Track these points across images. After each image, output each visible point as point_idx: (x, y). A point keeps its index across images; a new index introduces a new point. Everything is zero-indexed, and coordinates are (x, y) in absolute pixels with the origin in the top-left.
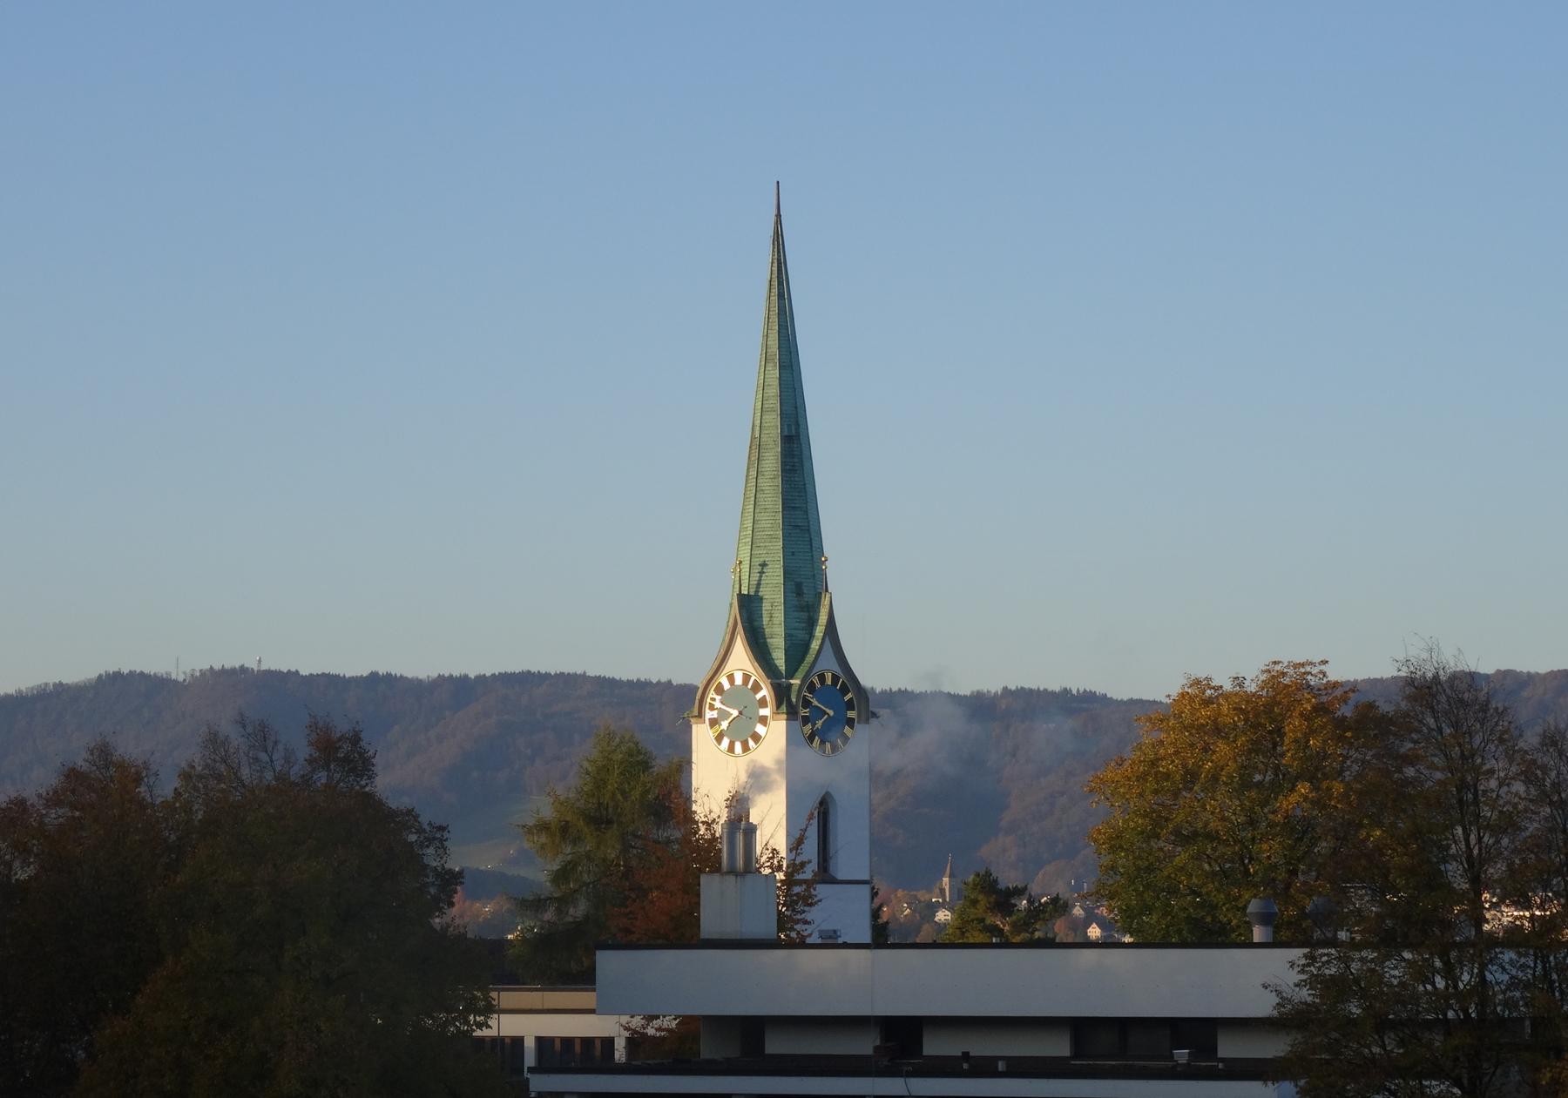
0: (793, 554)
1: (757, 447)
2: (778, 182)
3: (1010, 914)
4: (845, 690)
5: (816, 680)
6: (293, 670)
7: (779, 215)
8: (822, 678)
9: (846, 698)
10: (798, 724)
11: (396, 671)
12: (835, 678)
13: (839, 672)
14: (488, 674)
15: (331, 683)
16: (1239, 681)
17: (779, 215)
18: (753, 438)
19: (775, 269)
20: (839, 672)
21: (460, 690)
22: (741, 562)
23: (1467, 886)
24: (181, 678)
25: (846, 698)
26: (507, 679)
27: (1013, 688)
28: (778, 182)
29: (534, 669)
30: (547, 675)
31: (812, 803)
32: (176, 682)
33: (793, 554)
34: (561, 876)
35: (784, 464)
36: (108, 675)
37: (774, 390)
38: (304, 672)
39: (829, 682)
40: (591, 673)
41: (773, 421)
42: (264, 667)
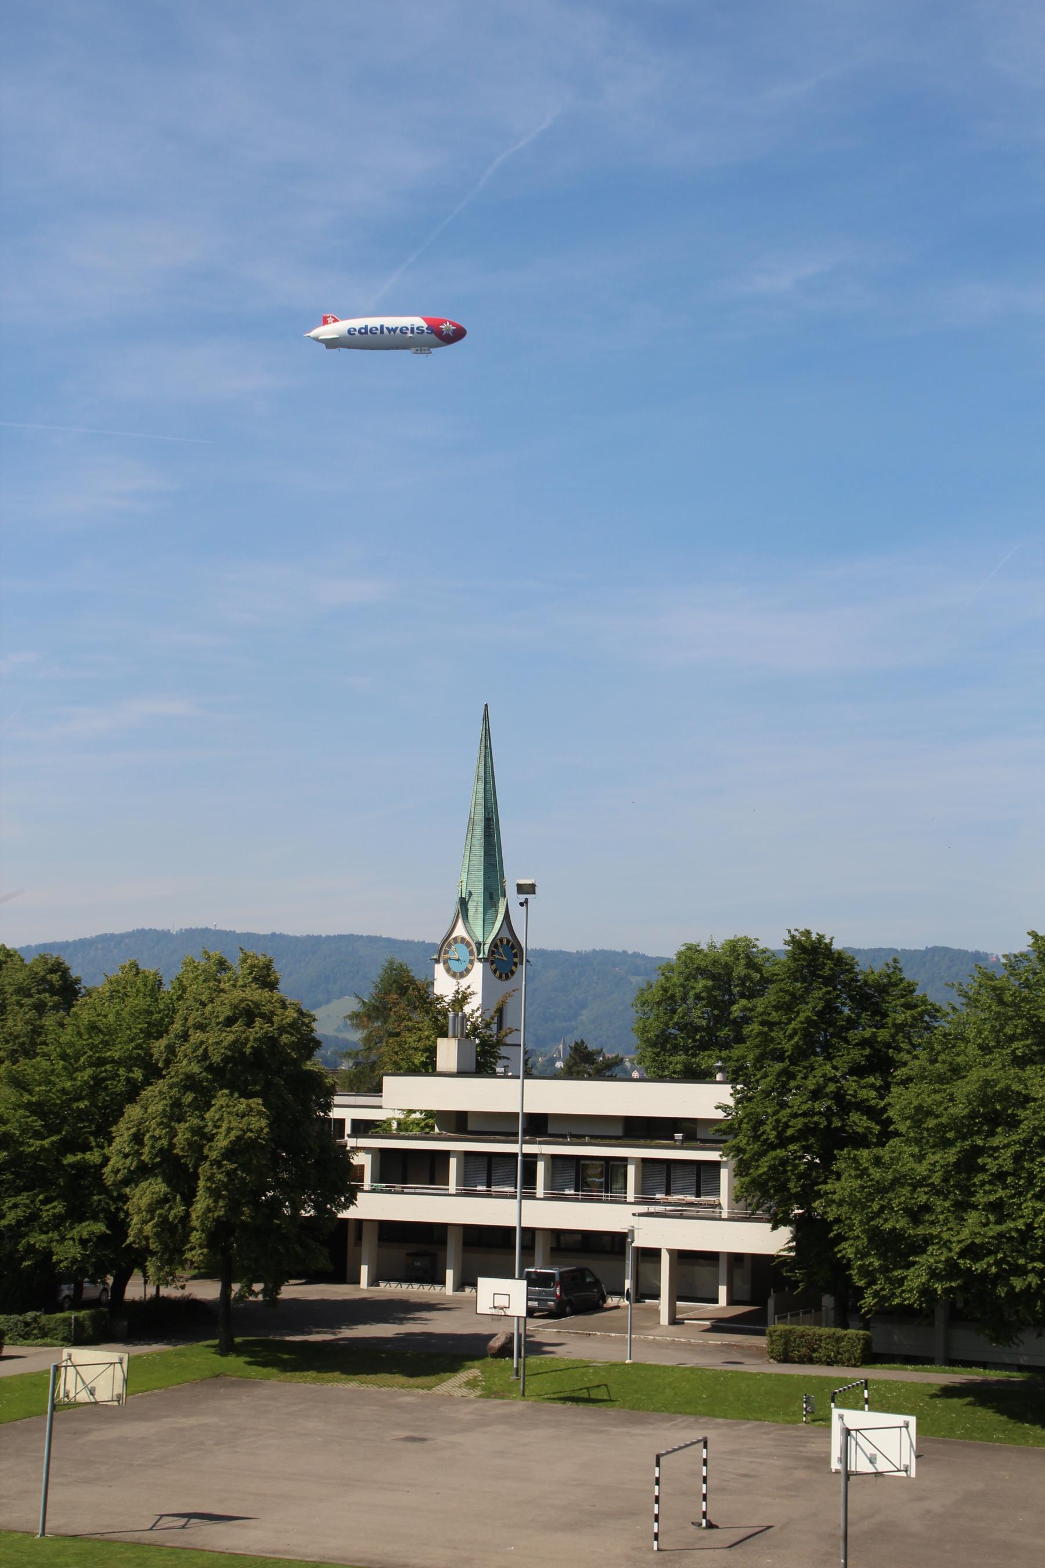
0: (489, 878)
1: (472, 822)
2: (486, 705)
3: (593, 1063)
4: (513, 948)
5: (499, 943)
6: (233, 930)
7: (487, 731)
8: (501, 941)
9: (514, 952)
10: (488, 964)
11: (285, 932)
12: (508, 941)
13: (510, 938)
14: (332, 935)
15: (250, 936)
16: (712, 946)
17: (487, 731)
18: (470, 819)
19: (484, 733)
20: (510, 938)
21: (315, 942)
22: (462, 882)
23: (264, 1122)
24: (175, 933)
25: (514, 952)
26: (340, 938)
27: (598, 950)
28: (486, 705)
29: (355, 933)
30: (362, 936)
31: (494, 1008)
32: (172, 935)
33: (489, 878)
34: (368, 1039)
35: (485, 832)
36: (137, 930)
37: (481, 795)
38: (238, 932)
39: (504, 976)
40: (384, 936)
41: (481, 810)
42: (217, 928)
